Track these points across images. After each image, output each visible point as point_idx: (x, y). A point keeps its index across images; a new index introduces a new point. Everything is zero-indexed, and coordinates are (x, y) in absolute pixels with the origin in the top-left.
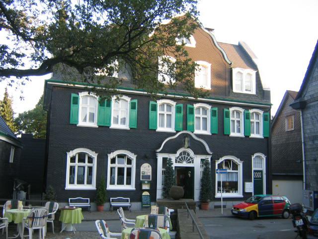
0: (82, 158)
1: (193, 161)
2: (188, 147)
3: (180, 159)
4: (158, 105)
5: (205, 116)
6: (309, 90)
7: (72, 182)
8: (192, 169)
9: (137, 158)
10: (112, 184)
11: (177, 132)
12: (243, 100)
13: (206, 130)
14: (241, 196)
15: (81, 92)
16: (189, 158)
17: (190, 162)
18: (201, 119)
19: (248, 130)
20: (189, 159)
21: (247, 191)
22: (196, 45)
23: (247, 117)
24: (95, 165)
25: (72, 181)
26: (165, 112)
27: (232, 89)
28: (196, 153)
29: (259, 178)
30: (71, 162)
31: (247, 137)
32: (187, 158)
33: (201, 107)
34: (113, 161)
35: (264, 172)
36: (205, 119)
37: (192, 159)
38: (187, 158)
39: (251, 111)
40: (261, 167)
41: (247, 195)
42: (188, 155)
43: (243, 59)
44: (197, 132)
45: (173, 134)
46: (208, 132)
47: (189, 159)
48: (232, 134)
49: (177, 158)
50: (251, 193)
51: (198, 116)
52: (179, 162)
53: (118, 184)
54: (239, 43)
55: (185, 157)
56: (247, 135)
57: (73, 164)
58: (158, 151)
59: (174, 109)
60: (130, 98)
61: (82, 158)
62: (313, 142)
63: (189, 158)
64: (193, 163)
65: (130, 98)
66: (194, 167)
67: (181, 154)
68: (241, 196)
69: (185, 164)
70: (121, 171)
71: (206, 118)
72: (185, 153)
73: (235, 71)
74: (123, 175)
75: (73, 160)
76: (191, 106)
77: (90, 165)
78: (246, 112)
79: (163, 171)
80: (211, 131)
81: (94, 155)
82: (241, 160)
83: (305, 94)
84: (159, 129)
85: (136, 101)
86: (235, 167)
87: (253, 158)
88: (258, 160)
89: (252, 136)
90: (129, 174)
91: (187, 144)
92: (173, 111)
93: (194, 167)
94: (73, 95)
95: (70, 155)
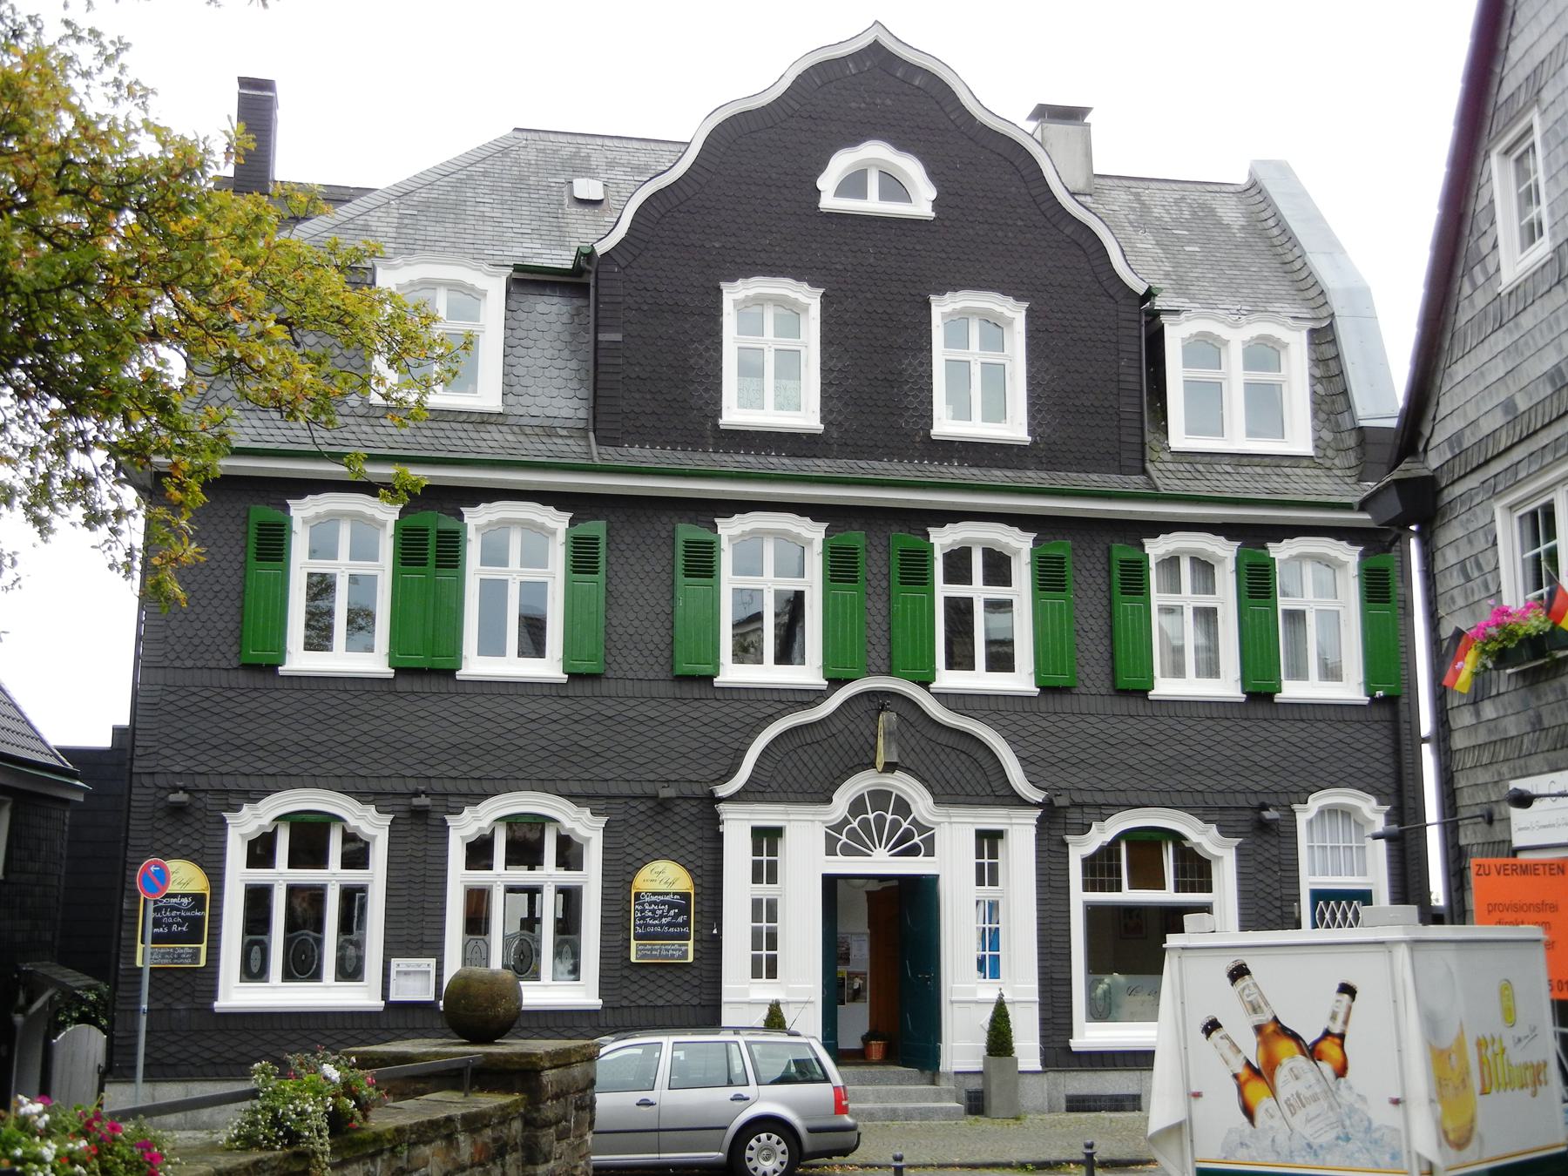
0: (525, 851)
2: (890, 767)
3: (853, 834)
5: (1206, 601)
6: (1443, 410)
7: (253, 971)
9: (607, 830)
11: (836, 683)
15: (475, 504)
16: (905, 825)
17: (913, 851)
20: (908, 835)
22: (936, 204)
23: (1257, 583)
24: (375, 878)
25: (255, 970)
28: (946, 795)
31: (1260, 696)
32: (895, 825)
33: (1185, 551)
34: (479, 853)
37: (923, 829)
38: (895, 825)
39: (1280, 551)
42: (903, 808)
44: (949, 680)
47: (908, 835)
49: (838, 828)
51: (1171, 600)
52: (848, 851)
53: (288, 976)
54: (1250, 174)
55: (880, 821)
56: (1262, 686)
57: (260, 876)
58: (723, 791)
59: (1022, 573)
60: (566, 516)
61: (309, 840)
62: (1477, 714)
63: (905, 825)
64: (930, 853)
65: (566, 516)
66: (937, 877)
67: (857, 807)
69: (882, 862)
70: (306, 904)
72: (880, 798)
73: (1175, 337)
74: (319, 925)
75: (479, 853)
77: (568, 878)
78: (1254, 554)
80: (391, 656)
81: (373, 825)
82: (1225, 831)
87: (1302, 819)
88: (1339, 836)
89: (1291, 691)
90: (568, 925)
93: (937, 877)
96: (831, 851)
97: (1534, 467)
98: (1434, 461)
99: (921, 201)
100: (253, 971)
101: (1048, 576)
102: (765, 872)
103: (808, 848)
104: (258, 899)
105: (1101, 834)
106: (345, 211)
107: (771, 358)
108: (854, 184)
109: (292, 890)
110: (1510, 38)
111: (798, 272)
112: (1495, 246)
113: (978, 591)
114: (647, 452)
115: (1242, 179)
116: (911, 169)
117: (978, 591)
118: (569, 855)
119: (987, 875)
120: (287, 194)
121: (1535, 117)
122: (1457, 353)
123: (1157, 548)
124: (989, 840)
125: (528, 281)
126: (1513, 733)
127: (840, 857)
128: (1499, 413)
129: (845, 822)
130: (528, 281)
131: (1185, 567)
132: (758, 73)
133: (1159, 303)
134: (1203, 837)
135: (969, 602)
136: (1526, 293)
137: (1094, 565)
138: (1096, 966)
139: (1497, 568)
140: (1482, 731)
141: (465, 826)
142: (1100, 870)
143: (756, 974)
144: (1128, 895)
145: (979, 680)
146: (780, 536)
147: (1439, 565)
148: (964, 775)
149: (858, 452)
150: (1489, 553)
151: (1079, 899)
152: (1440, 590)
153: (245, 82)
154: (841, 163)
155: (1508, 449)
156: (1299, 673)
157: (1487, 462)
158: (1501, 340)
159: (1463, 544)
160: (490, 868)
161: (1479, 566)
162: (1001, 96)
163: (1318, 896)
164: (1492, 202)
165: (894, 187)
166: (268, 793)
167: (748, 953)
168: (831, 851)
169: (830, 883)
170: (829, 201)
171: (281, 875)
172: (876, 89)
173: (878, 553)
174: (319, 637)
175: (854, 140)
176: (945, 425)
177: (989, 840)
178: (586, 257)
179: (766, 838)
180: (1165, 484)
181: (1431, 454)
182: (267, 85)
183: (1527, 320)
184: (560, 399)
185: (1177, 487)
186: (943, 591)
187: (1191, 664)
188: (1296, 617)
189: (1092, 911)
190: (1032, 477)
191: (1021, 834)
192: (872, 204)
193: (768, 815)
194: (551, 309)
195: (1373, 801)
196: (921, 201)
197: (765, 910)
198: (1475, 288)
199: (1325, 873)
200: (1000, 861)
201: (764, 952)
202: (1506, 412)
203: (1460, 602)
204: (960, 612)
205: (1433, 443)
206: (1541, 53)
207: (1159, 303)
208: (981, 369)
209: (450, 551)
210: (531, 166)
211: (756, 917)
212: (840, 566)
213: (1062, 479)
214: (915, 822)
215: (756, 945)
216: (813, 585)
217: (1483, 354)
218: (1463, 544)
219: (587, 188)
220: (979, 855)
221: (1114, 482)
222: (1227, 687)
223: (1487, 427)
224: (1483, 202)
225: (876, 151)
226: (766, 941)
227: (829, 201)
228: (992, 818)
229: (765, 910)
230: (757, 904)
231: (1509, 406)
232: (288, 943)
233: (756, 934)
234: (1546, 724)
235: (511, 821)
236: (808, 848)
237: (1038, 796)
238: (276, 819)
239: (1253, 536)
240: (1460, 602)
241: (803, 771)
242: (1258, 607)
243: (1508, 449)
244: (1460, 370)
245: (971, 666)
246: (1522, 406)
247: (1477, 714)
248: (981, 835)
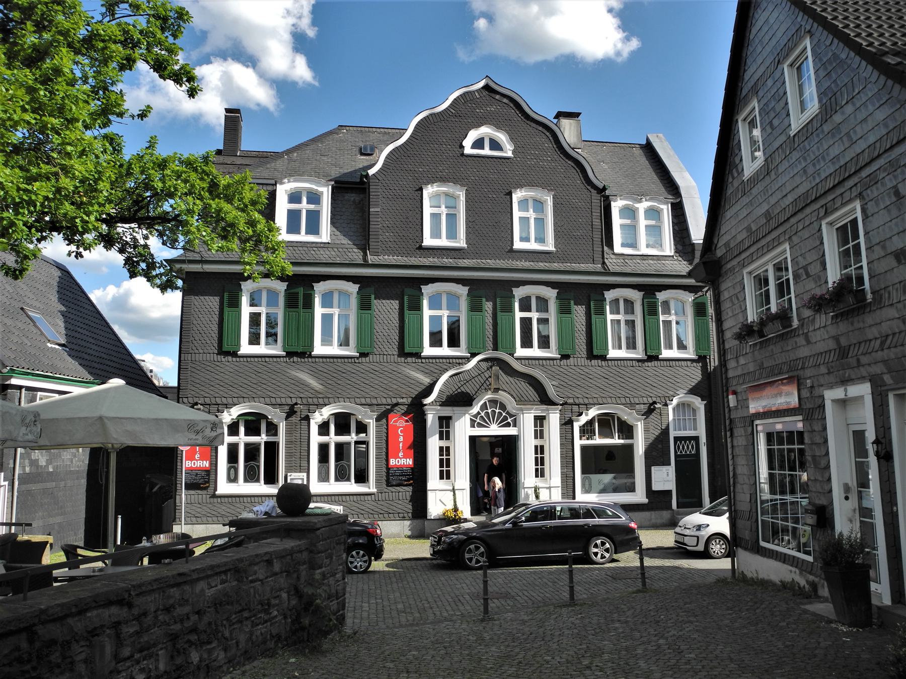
1: (515, 422)
6: (722, 232)
7: (232, 479)
10: (323, 481)
11: (474, 355)
13: (634, 348)
14: (645, 500)
17: (508, 425)
20: (505, 418)
21: (656, 487)
22: (514, 152)
23: (651, 310)
29: (691, 455)
30: (320, 434)
32: (500, 414)
34: (324, 429)
35: (703, 439)
36: (631, 324)
37: (511, 416)
40: (695, 429)
41: (657, 499)
42: (503, 407)
43: (657, 174)
44: (521, 352)
47: (505, 418)
49: (476, 416)
50: (669, 492)
52: (480, 425)
53: (337, 480)
57: (324, 439)
59: (553, 306)
61: (343, 423)
62: (738, 362)
67: (484, 407)
68: (645, 500)
69: (494, 430)
71: (633, 322)
72: (493, 402)
73: (616, 206)
75: (324, 429)
79: (536, 447)
83: (716, 242)
96: (473, 426)
97: (760, 254)
100: (324, 477)
102: (445, 435)
104: (324, 449)
107: (441, 217)
108: (479, 144)
109: (247, 445)
110: (745, 71)
111: (545, 185)
112: (741, 160)
113: (534, 315)
114: (436, 260)
116: (502, 137)
117: (534, 315)
118: (272, 429)
119: (539, 434)
121: (755, 103)
122: (727, 207)
124: (540, 420)
126: (752, 370)
127: (477, 428)
128: (744, 231)
129: (479, 413)
133: (607, 193)
135: (530, 319)
136: (755, 179)
138: (584, 471)
139: (745, 299)
140: (740, 369)
141: (317, 418)
142: (587, 430)
143: (441, 478)
144: (598, 441)
145: (535, 352)
147: (722, 298)
149: (564, 261)
150: (742, 293)
151: (578, 443)
152: (722, 309)
154: (473, 135)
155: (749, 247)
157: (740, 253)
158: (745, 200)
159: (731, 289)
160: (238, 435)
161: (738, 299)
163: (676, 439)
164: (739, 141)
166: (236, 405)
167: (438, 469)
168: (473, 426)
169: (473, 439)
170: (468, 150)
171: (333, 439)
174: (254, 339)
175: (478, 126)
176: (518, 245)
177: (540, 420)
180: (612, 268)
181: (718, 251)
182: (237, 111)
183: (755, 191)
185: (618, 269)
186: (519, 315)
189: (584, 449)
191: (554, 419)
193: (446, 411)
195: (699, 399)
197: (445, 451)
198: (733, 178)
199: (680, 430)
200: (451, 430)
201: (445, 469)
202: (747, 232)
203: (730, 314)
204: (526, 324)
205: (718, 246)
206: (756, 77)
207: (607, 193)
208: (532, 222)
211: (441, 454)
212: (475, 307)
214: (508, 413)
215: (441, 465)
216: (280, 312)
217: (737, 207)
218: (731, 289)
220: (536, 426)
223: (739, 238)
224: (736, 142)
225: (485, 131)
226: (445, 464)
227: (468, 150)
229: (445, 451)
230: (441, 449)
231: (748, 228)
232: (245, 467)
233: (441, 461)
234: (765, 366)
235: (337, 416)
238: (239, 416)
240: (730, 314)
243: (749, 247)
244: (728, 214)
245: (441, 345)
246: (754, 229)
247: (738, 362)
248: (536, 418)
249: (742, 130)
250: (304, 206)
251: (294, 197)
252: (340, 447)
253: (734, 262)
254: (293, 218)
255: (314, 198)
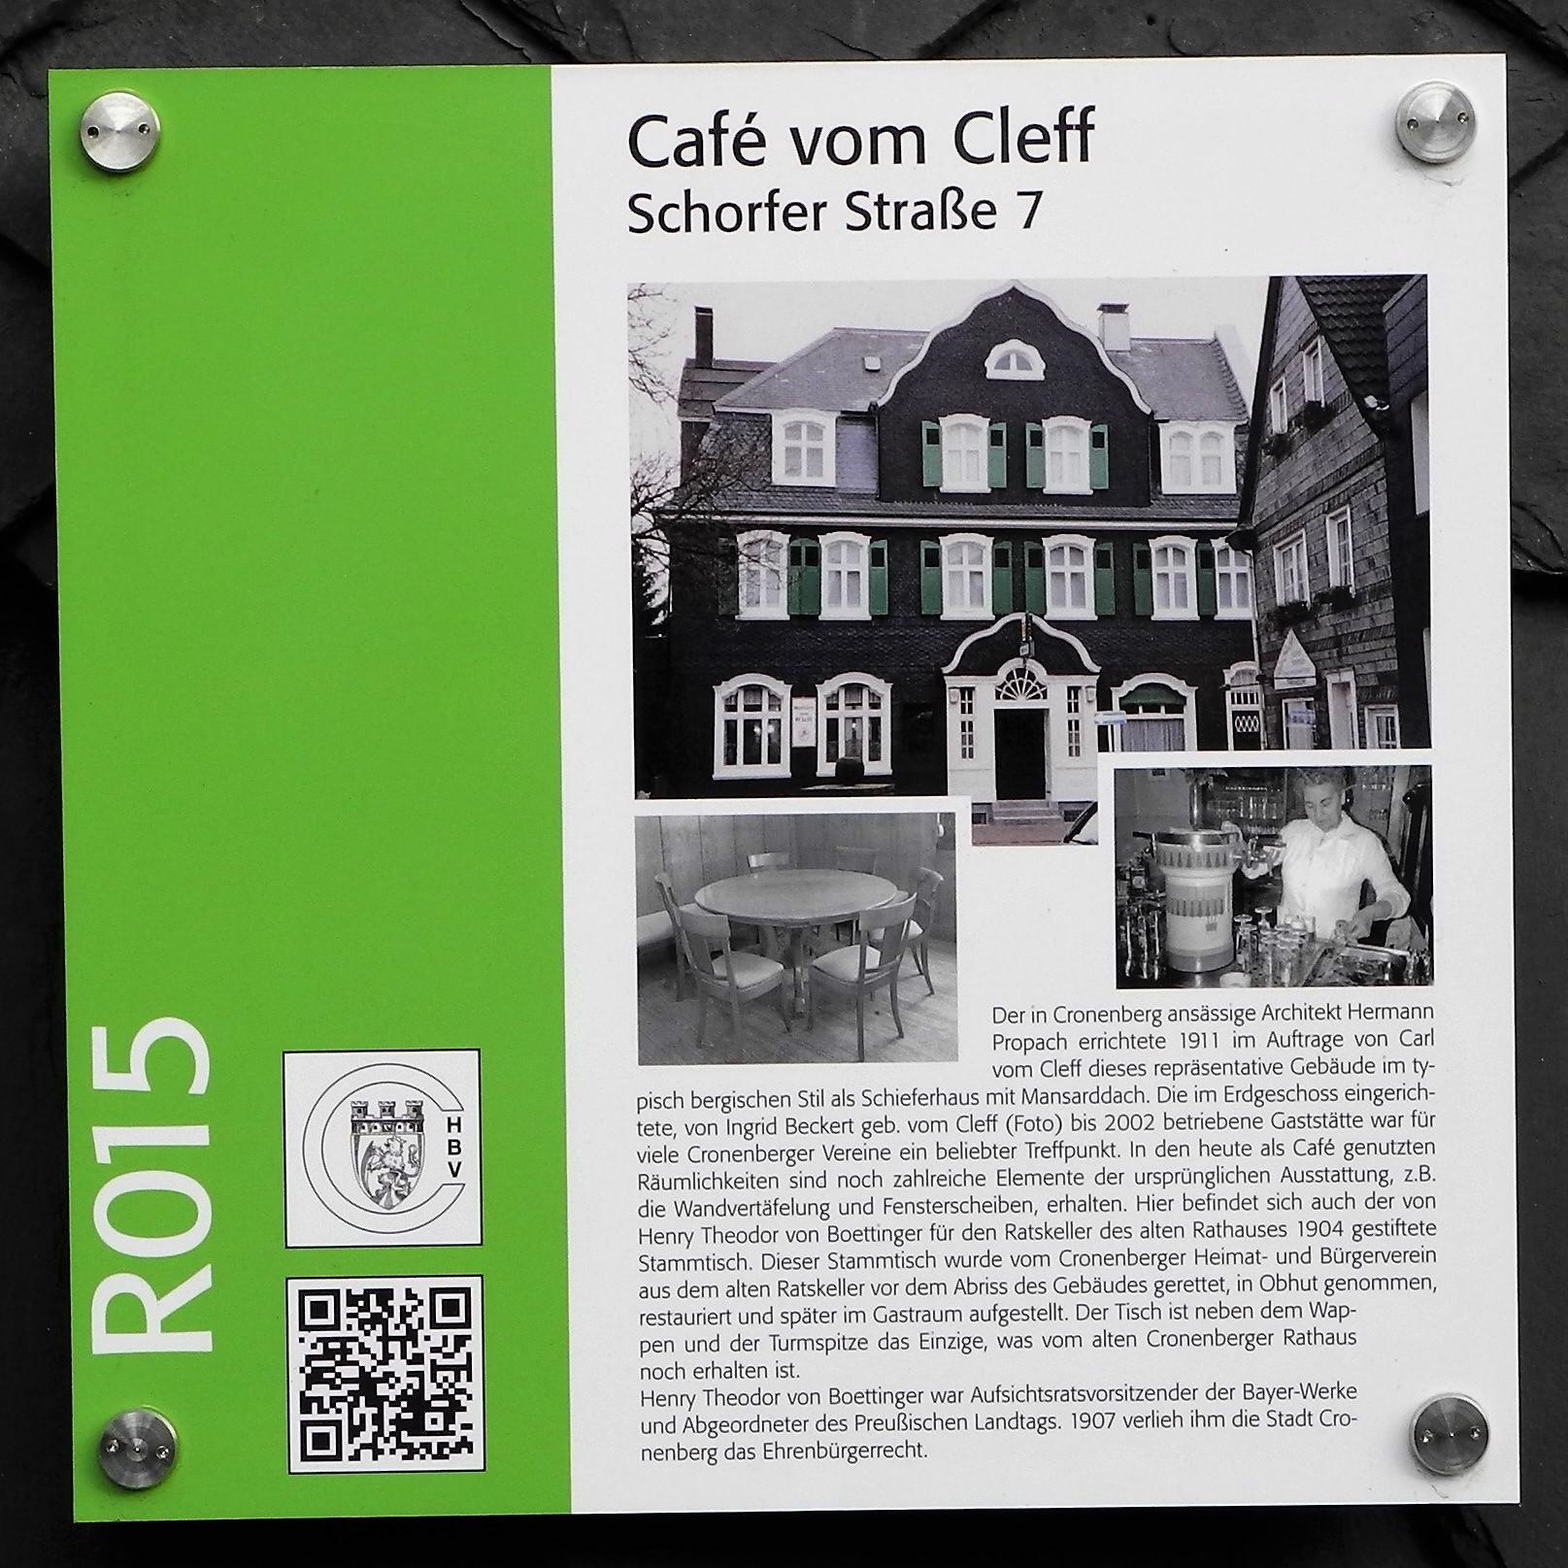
1: (1045, 693)
4: (1047, 551)
7: (731, 760)
8: (1040, 716)
11: (998, 617)
12: (1186, 514)
17: (1037, 697)
18: (1233, 577)
19: (1207, 597)
23: (1205, 560)
26: (967, 568)
27: (1159, 481)
28: (1051, 671)
31: (1207, 617)
42: (1032, 676)
44: (1054, 612)
45: (988, 624)
46: (1088, 613)
48: (1160, 614)
51: (1224, 570)
52: (1006, 697)
58: (946, 670)
67: (1010, 676)
69: (1021, 703)
71: (1184, 576)
72: (1021, 672)
76: (932, 545)
84: (949, 613)
85: (883, 544)
86: (1177, 704)
91: (1024, 649)
92: (1088, 567)
94: (925, 545)
95: (722, 691)
98: (1255, 522)
99: (1037, 371)
101: (1101, 560)
103: (987, 696)
104: (731, 726)
105: (1129, 686)
106: (753, 382)
107: (964, 454)
108: (1004, 363)
115: (1210, 337)
116: (1032, 353)
120: (726, 367)
123: (1155, 544)
124: (1074, 691)
125: (848, 417)
130: (848, 417)
131: (1170, 551)
132: (956, 312)
134: (1179, 686)
137: (1124, 561)
146: (971, 544)
148: (1061, 660)
153: (698, 309)
154: (997, 352)
156: (1228, 603)
162: (1079, 315)
163: (1235, 714)
165: (1023, 364)
170: (992, 373)
172: (1016, 313)
173: (1019, 560)
178: (873, 406)
179: (967, 692)
184: (865, 481)
187: (1173, 601)
188: (1226, 576)
190: (1094, 511)
192: (1013, 373)
193: (966, 681)
194: (859, 432)
196: (1037, 371)
197: (967, 727)
208: (1069, 457)
209: (814, 557)
210: (844, 344)
213: (1109, 510)
219: (873, 363)
221: (1134, 511)
222: (1191, 613)
225: (1015, 344)
227: (992, 373)
228: (1075, 680)
229: (967, 727)
236: (987, 696)
237: (1097, 669)
239: (1204, 537)
241: (983, 661)
242: (1207, 572)
249: (1273, 396)
250: (804, 443)
251: (793, 430)
252: (749, 725)
253: (1265, 536)
254: (792, 453)
255: (816, 431)
